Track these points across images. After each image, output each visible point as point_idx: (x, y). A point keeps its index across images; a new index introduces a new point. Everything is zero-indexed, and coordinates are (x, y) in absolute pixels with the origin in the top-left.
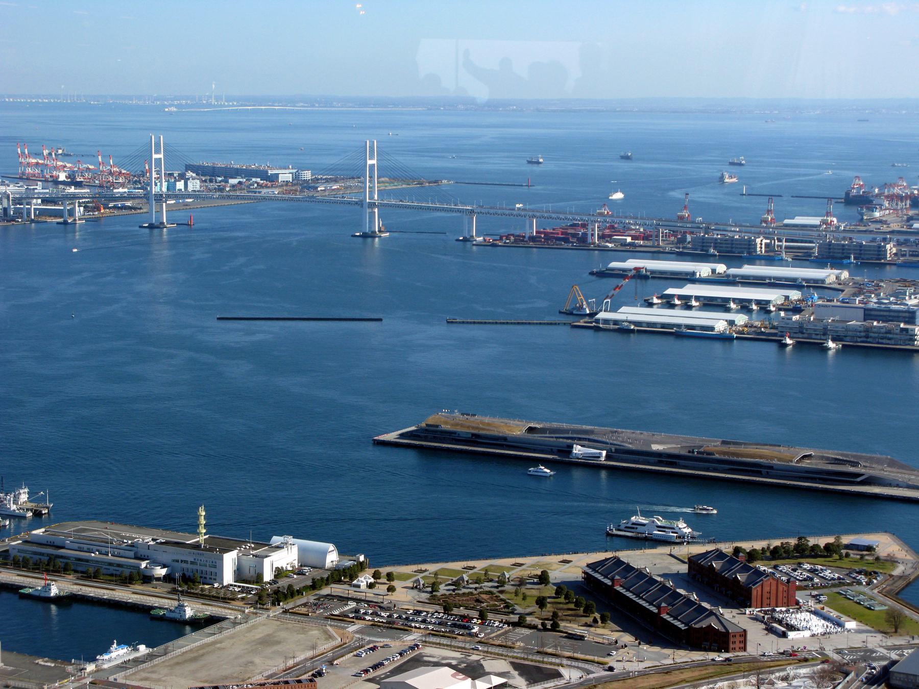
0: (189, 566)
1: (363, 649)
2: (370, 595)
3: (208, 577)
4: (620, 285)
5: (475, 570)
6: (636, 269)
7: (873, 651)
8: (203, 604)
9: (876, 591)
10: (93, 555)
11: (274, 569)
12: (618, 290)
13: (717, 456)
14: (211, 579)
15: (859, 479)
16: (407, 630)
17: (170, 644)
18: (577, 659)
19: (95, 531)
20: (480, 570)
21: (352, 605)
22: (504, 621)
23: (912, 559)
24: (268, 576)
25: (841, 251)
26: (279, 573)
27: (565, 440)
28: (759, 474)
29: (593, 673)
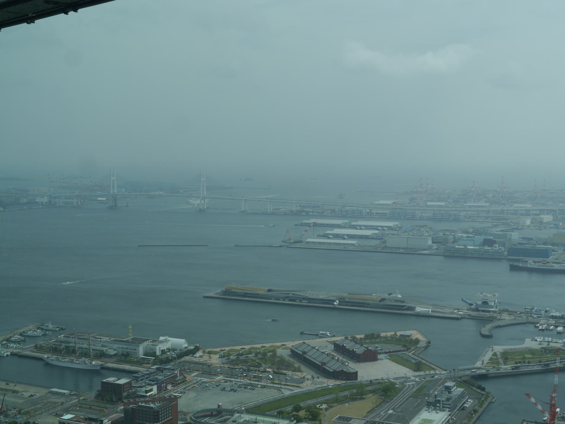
0: (125, 350)
1: (198, 383)
2: (202, 360)
3: (133, 354)
4: (307, 229)
5: (245, 349)
6: (313, 223)
7: (410, 378)
8: (131, 366)
9: (411, 354)
10: (84, 345)
11: (161, 350)
12: (303, 233)
13: (347, 300)
14: (134, 355)
15: (404, 308)
16: (217, 375)
17: (112, 382)
18: (288, 385)
19: (86, 336)
20: (247, 349)
21: (238, 369)
22: (257, 370)
23: (425, 340)
24: (158, 353)
25: (456, 216)
26: (163, 352)
27: (283, 295)
28: (364, 307)
29: (294, 391)
